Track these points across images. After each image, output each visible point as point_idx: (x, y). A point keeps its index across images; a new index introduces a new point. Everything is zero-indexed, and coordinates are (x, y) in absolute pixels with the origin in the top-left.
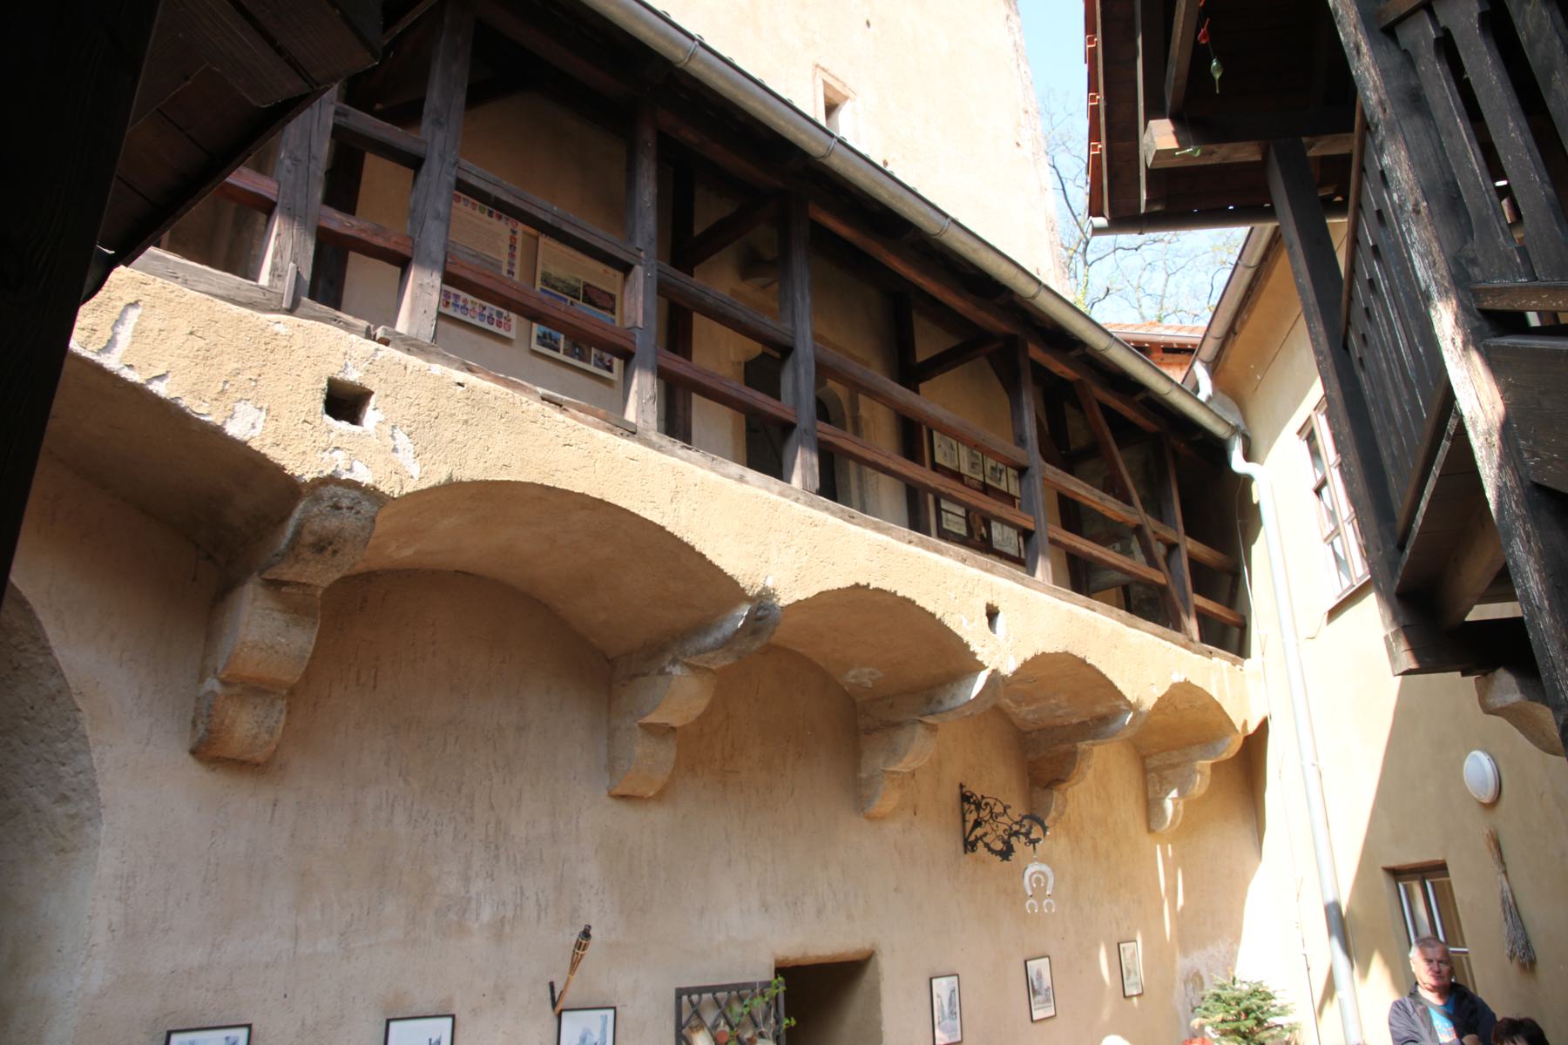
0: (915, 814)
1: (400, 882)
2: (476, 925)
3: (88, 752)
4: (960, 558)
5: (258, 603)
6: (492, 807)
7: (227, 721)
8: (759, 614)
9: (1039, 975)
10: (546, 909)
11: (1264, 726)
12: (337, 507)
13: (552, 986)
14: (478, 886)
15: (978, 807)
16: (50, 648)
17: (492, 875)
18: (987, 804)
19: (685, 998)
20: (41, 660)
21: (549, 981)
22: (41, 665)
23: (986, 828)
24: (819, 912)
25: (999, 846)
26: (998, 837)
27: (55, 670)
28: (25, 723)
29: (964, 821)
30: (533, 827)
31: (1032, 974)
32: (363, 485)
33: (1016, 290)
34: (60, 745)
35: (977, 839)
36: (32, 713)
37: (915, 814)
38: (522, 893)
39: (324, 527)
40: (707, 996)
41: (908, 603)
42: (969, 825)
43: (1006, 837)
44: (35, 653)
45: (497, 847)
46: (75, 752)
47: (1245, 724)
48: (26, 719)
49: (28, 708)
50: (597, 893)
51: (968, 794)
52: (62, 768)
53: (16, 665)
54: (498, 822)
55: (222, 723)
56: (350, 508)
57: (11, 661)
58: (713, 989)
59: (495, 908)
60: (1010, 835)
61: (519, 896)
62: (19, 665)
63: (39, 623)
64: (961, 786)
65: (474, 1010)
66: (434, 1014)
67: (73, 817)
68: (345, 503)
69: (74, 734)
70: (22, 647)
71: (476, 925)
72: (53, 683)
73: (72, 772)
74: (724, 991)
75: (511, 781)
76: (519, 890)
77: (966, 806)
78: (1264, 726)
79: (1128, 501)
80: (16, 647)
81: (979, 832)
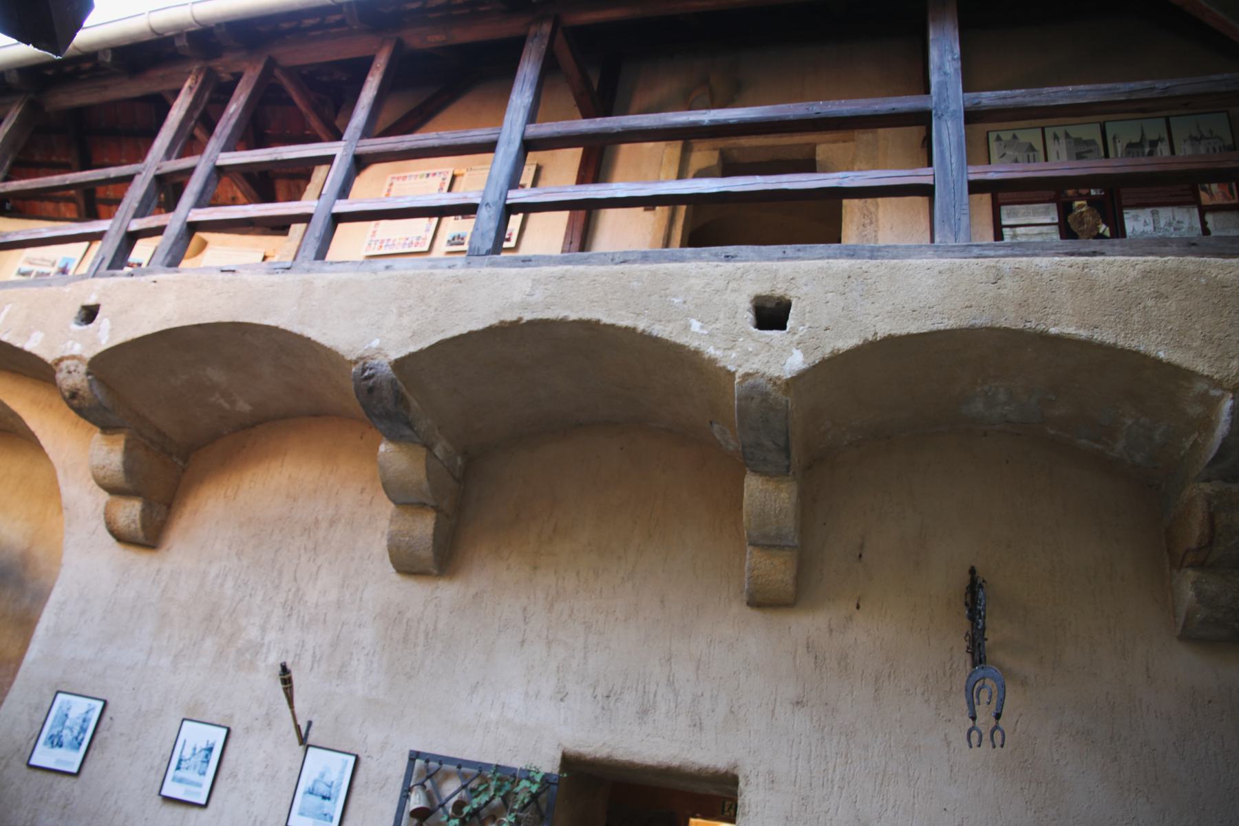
0: (858, 607)
1: (218, 627)
2: (263, 665)
4: (533, 259)
6: (295, 579)
7: (113, 517)
8: (366, 374)
10: (319, 660)
12: (70, 372)
17: (283, 629)
21: (309, 719)
24: (644, 712)
30: (324, 595)
33: (96, 48)
37: (858, 607)
38: (303, 646)
39: (68, 386)
41: (591, 326)
50: (368, 654)
56: (75, 371)
58: (460, 763)
59: (280, 655)
61: (300, 648)
65: (247, 728)
66: (217, 723)
68: (72, 368)
71: (263, 665)
74: (454, 765)
75: (314, 560)
76: (301, 644)
79: (129, 179)
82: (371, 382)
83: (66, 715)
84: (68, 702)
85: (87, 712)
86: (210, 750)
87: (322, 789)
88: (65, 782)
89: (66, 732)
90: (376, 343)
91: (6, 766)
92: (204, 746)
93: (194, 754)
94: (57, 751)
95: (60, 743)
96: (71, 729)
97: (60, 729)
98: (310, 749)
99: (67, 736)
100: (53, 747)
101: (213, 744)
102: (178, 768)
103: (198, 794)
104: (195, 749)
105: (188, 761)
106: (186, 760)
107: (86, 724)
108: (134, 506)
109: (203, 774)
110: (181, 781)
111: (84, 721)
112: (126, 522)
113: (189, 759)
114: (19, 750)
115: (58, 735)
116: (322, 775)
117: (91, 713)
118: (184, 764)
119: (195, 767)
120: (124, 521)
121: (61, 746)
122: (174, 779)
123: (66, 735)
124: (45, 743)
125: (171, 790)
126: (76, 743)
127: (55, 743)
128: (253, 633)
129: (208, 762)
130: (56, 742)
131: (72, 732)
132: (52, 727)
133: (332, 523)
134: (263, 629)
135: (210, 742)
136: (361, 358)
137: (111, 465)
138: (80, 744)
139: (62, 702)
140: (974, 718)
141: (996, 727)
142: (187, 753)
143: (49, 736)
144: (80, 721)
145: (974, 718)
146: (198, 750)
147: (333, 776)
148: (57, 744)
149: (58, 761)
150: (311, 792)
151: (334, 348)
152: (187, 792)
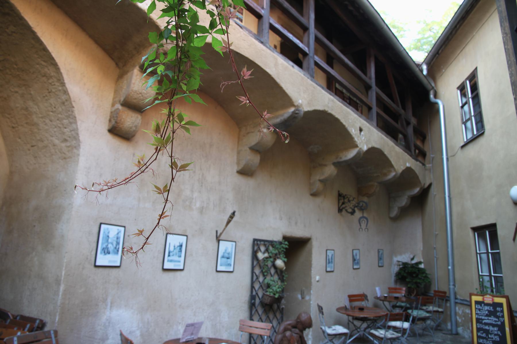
3: (76, 123)
5: (138, 77)
6: (201, 169)
7: (122, 120)
9: (356, 255)
11: (430, 185)
13: (217, 232)
14: (196, 195)
15: (344, 197)
16: (64, 83)
18: (347, 197)
19: (256, 242)
20: (60, 88)
22: (60, 90)
23: (347, 205)
24: (296, 223)
25: (350, 210)
26: (351, 208)
27: (66, 92)
28: (51, 113)
29: (339, 203)
31: (354, 254)
32: (198, 24)
34: (65, 121)
35: (343, 208)
36: (54, 109)
40: (262, 243)
42: (340, 204)
43: (353, 208)
44: (58, 86)
45: (202, 183)
46: (71, 123)
47: (424, 184)
48: (52, 112)
49: (53, 107)
51: (341, 194)
52: (65, 130)
53: (50, 91)
54: (203, 175)
55: (121, 120)
57: (48, 90)
58: (264, 241)
60: (355, 207)
62: (51, 91)
63: (61, 73)
64: (339, 191)
67: (68, 147)
69: (71, 117)
70: (53, 84)
72: (64, 97)
73: (69, 131)
77: (340, 198)
78: (430, 185)
80: (50, 83)
81: (344, 206)
82: (296, 115)
83: (108, 236)
84: (108, 229)
85: (118, 234)
86: (181, 246)
87: (226, 255)
88: (114, 270)
89: (110, 246)
90: (300, 101)
91: (83, 268)
92: (178, 244)
93: (175, 249)
94: (108, 256)
95: (108, 252)
96: (112, 244)
97: (106, 244)
98: (221, 242)
99: (111, 247)
100: (105, 254)
101: (182, 243)
102: (169, 256)
103: (180, 265)
104: (175, 246)
105: (173, 252)
106: (172, 252)
107: (118, 240)
108: (137, 117)
109: (180, 256)
110: (171, 261)
111: (118, 238)
112: (131, 126)
113: (173, 251)
114: (87, 259)
115: (106, 248)
116: (226, 250)
117: (119, 234)
118: (171, 254)
119: (176, 254)
120: (130, 124)
121: (109, 253)
122: (168, 261)
123: (110, 247)
124: (101, 253)
125: (167, 266)
126: (116, 251)
127: (106, 252)
128: (188, 193)
129: (181, 251)
130: (106, 251)
131: (113, 245)
132: (102, 244)
133: (211, 146)
134: (192, 191)
135: (181, 243)
136: (298, 106)
137: (146, 94)
138: (118, 251)
139: (104, 230)
140: (361, 226)
141: (366, 228)
142: (172, 249)
143: (102, 248)
144: (115, 239)
145: (361, 226)
146: (176, 246)
147: (229, 250)
148: (107, 252)
149: (110, 261)
150: (223, 257)
151: (291, 97)
152: (175, 265)
